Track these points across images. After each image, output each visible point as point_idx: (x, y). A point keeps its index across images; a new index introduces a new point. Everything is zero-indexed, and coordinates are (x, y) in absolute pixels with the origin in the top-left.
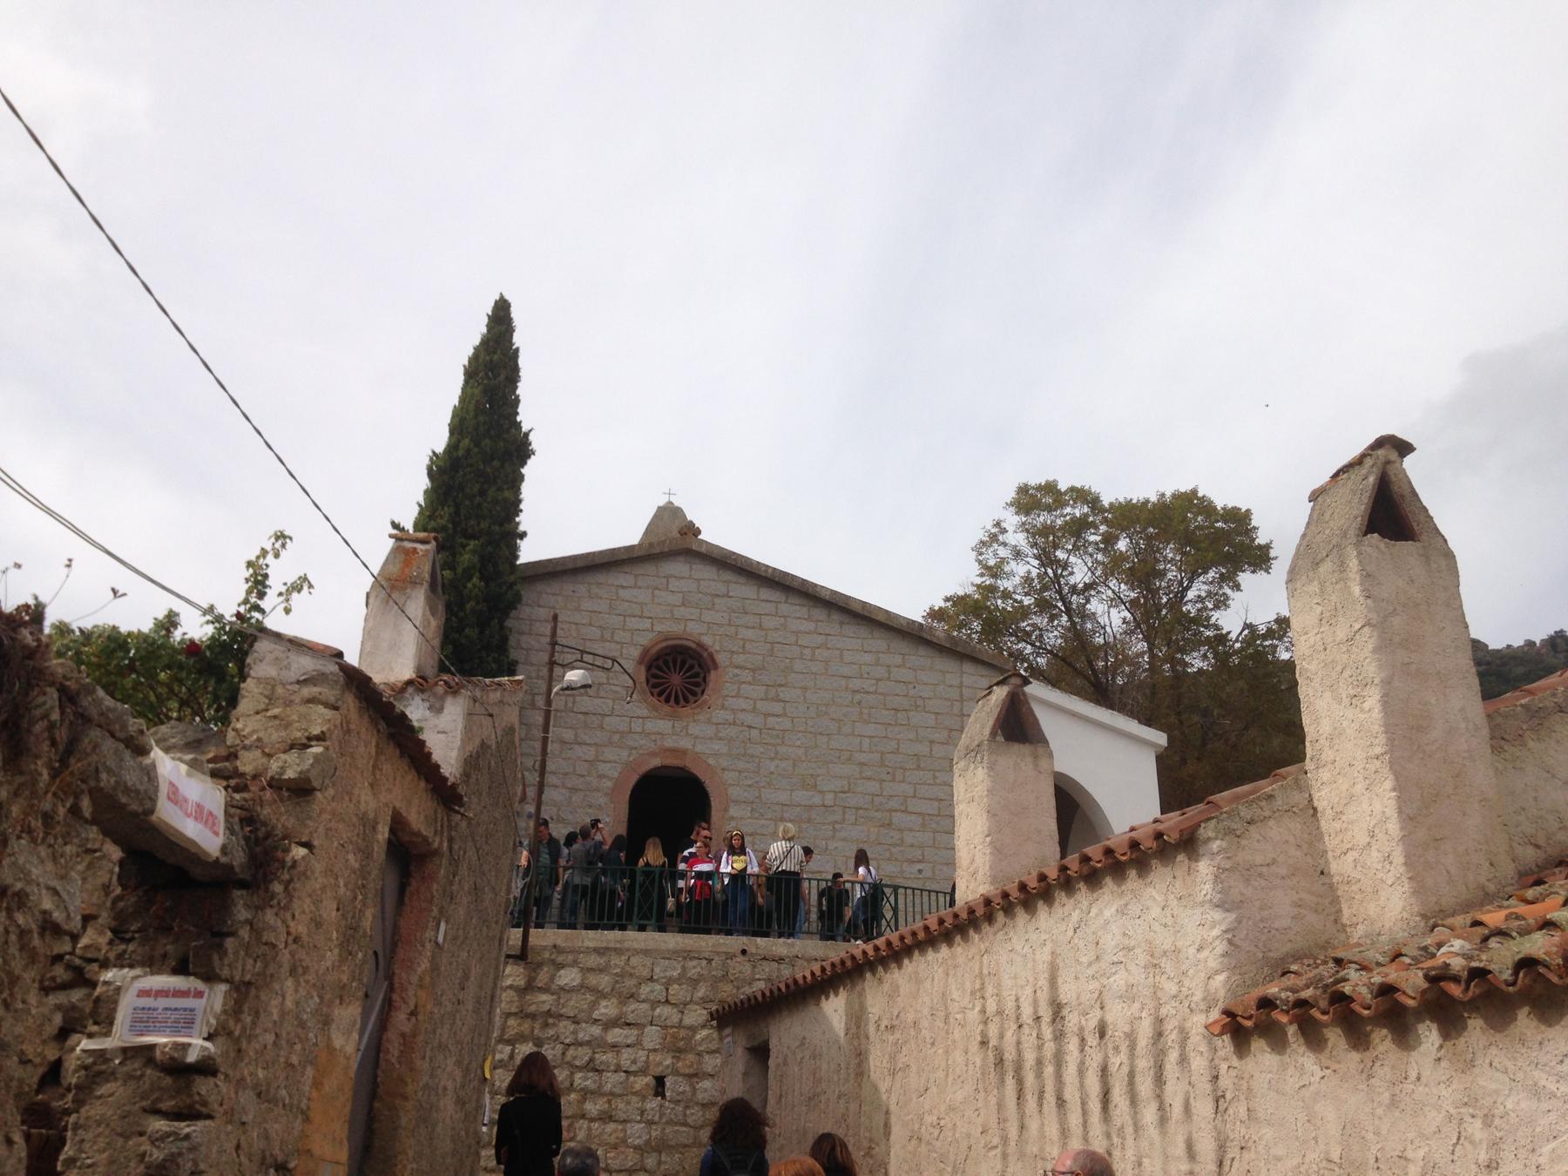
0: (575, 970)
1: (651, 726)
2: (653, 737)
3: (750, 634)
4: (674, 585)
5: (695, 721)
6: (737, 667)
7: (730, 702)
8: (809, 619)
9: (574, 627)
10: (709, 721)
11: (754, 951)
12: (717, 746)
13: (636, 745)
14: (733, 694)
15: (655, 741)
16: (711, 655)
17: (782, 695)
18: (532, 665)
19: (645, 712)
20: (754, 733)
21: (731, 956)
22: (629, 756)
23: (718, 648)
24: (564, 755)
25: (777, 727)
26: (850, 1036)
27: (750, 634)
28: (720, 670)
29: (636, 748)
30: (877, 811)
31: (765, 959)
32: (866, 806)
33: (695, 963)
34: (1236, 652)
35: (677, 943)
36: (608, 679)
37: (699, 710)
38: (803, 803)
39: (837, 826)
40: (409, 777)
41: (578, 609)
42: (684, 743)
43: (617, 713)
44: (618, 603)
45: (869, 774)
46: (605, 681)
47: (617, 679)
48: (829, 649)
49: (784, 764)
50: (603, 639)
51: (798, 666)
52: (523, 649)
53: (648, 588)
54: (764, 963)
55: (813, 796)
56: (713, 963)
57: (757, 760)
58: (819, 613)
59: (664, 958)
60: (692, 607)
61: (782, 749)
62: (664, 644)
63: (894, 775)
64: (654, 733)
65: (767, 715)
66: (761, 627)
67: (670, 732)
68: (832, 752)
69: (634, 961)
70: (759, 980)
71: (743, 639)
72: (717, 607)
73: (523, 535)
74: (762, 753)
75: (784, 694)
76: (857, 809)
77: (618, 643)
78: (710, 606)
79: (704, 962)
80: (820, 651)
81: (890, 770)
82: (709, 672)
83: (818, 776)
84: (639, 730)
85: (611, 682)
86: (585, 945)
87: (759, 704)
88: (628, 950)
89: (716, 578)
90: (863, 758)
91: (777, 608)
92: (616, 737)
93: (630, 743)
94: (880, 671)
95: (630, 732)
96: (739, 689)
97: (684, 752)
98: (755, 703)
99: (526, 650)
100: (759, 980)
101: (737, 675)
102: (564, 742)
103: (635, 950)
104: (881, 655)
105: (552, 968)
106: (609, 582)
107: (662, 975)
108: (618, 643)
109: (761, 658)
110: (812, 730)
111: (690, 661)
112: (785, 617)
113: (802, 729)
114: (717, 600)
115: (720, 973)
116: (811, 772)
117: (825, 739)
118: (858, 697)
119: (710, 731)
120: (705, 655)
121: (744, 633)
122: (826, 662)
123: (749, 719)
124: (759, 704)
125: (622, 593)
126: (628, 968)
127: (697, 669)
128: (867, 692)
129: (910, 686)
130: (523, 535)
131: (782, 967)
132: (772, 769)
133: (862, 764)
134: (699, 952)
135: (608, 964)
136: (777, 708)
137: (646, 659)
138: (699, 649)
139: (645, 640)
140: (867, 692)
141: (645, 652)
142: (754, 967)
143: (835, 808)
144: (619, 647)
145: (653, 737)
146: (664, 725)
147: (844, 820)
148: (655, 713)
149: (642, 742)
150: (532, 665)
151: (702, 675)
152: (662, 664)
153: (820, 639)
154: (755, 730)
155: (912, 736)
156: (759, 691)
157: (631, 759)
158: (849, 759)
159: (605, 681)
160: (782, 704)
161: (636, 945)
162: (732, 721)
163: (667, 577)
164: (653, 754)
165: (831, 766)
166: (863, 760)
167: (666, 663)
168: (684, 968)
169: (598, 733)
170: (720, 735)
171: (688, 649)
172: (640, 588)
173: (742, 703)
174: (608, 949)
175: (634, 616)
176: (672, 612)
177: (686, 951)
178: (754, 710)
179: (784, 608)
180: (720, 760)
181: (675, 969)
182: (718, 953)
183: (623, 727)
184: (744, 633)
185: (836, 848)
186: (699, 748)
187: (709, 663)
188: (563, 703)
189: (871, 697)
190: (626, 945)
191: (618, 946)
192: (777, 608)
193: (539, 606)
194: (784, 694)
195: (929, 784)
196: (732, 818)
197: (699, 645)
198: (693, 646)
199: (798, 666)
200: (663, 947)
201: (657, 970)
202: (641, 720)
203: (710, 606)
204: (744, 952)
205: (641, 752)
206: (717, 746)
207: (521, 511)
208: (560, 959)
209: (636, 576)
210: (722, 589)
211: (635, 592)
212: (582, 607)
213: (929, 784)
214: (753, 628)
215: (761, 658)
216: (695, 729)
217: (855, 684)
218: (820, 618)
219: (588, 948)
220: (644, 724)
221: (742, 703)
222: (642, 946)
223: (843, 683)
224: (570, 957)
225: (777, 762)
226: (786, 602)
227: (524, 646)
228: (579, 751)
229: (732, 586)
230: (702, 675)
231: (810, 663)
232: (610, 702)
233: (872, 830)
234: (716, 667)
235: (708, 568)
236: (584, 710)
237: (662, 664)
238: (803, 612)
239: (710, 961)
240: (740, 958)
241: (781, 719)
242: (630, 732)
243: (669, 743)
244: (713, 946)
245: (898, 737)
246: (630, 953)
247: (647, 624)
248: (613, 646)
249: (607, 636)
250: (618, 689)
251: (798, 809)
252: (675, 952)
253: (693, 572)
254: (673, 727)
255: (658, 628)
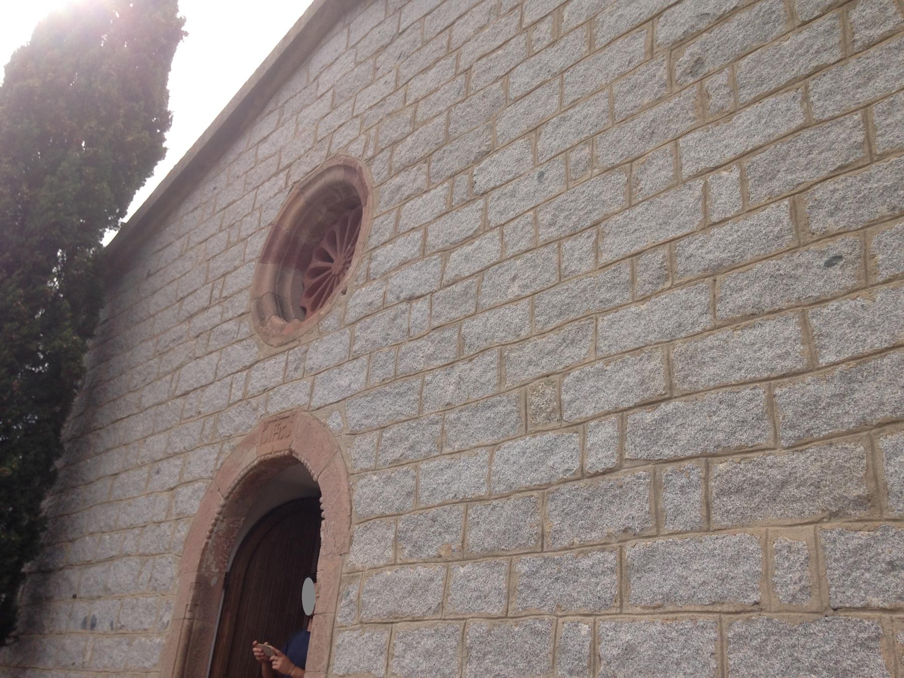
26: (473, 241)
30: (798, 446)
32: (744, 437)
34: (59, 291)
38: (523, 483)
39: (633, 550)
40: (139, 426)
45: (746, 297)
55: (550, 451)
62: (301, 202)
63: (866, 257)
74: (430, 357)
76: (708, 457)
81: (838, 246)
117: (584, 243)
118: (686, 56)
133: (714, 272)
143: (625, 477)
147: (657, 515)
185: (629, 650)
196: (354, 574)
207: (165, 149)
233: (784, 539)
251: (508, 508)
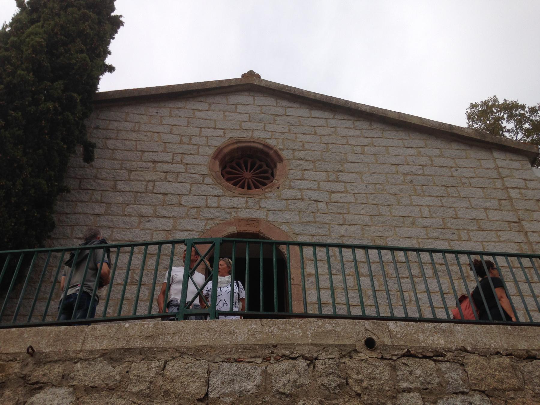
0: (63, 391)
1: (226, 202)
2: (228, 210)
3: (308, 138)
4: (240, 109)
5: (266, 197)
6: (299, 160)
7: (297, 183)
8: (355, 128)
9: (156, 135)
10: (279, 198)
11: (387, 341)
12: (288, 216)
13: (212, 217)
14: (299, 178)
15: (230, 213)
16: (276, 152)
17: (341, 178)
18: (116, 160)
19: (220, 192)
20: (321, 206)
21: (351, 352)
22: (205, 225)
23: (281, 147)
24: (141, 227)
25: (341, 200)
27: (308, 138)
28: (284, 161)
29: (212, 219)
31: (409, 355)
33: (286, 365)
35: (251, 333)
36: (186, 169)
37: (269, 189)
41: (160, 123)
42: (256, 214)
43: (194, 193)
44: (194, 120)
46: (183, 170)
47: (194, 169)
48: (375, 146)
49: (353, 229)
50: (181, 142)
51: (351, 157)
52: (108, 149)
53: (220, 111)
54: (410, 361)
56: (319, 365)
57: (327, 226)
58: (363, 124)
59: (228, 360)
60: (257, 122)
61: (350, 217)
62: (236, 146)
64: (229, 208)
65: (331, 192)
66: (315, 134)
67: (244, 206)
68: (394, 218)
69: (172, 369)
70: (408, 390)
71: (302, 141)
72: (277, 122)
73: (110, 53)
74: (331, 220)
75: (343, 177)
77: (196, 145)
78: (272, 122)
79: (302, 364)
80: (369, 147)
81: (454, 231)
82: (275, 166)
83: (387, 237)
84: (216, 205)
85: (189, 171)
86: (88, 347)
87: (322, 185)
88: (164, 350)
89: (275, 105)
90: (425, 222)
91: (327, 122)
92: (193, 211)
93: (208, 215)
94: (424, 160)
95: (207, 206)
96: (303, 174)
97: (257, 221)
98: (319, 184)
99: (113, 150)
100: (408, 390)
101: (301, 165)
102: (143, 216)
103: (177, 350)
104: (421, 149)
105: (21, 391)
106: (188, 107)
107: (227, 390)
108: (196, 145)
109: (319, 153)
110: (374, 202)
111: (258, 163)
112: (335, 127)
113: (364, 201)
114: (277, 118)
115: (334, 381)
116: (379, 234)
118: (408, 178)
119: (281, 205)
120: (271, 152)
121: (301, 137)
122: (375, 155)
123: (315, 195)
124: (322, 185)
125: (198, 114)
126: (160, 381)
127: (265, 167)
128: (416, 175)
129: (454, 169)
130: (110, 53)
131: (444, 367)
132: (343, 232)
134: (291, 346)
135: (125, 376)
136: (339, 187)
137: (220, 156)
138: (266, 149)
139: (219, 142)
140: (416, 175)
141: (220, 150)
142: (394, 368)
144: (195, 147)
145: (228, 210)
146: (239, 201)
148: (230, 193)
149: (217, 214)
150: (116, 160)
151: (270, 172)
152: (235, 165)
153: (367, 141)
154: (321, 203)
155: (464, 204)
156: (322, 176)
157: (208, 227)
158: (413, 223)
159: (183, 170)
160: (343, 184)
161: (177, 342)
162: (300, 197)
163: (236, 105)
164: (230, 224)
165: (397, 229)
166: (427, 224)
167: (239, 165)
168: (265, 373)
169: (177, 209)
170: (290, 207)
171: (256, 150)
172: (213, 111)
173: (306, 184)
174: (127, 351)
175: (209, 128)
176: (240, 125)
177: (267, 346)
178: (319, 189)
179: (333, 122)
180: (292, 227)
181: (249, 377)
182: (325, 348)
183: (201, 203)
184: (301, 137)
186: (271, 218)
187: (276, 158)
188: (144, 187)
189: (420, 178)
190: (161, 343)
191: (147, 344)
192: (327, 122)
193: (126, 121)
194: (343, 177)
195: (495, 242)
197: (265, 145)
198: (260, 147)
199: (351, 157)
200: (226, 340)
201: (216, 381)
202: (216, 198)
203: (272, 122)
204: (370, 344)
205: (217, 222)
206: (288, 216)
208: (38, 374)
209: (210, 104)
210: (281, 111)
211: (209, 113)
212: (164, 122)
213: (495, 242)
214: (310, 134)
215: (319, 153)
216: (266, 204)
217: (406, 169)
218: (364, 127)
219: (91, 352)
220: (219, 201)
221: (306, 184)
222: (190, 341)
223: (393, 168)
224: (58, 369)
225: (345, 227)
226: (334, 118)
227: (110, 147)
228: (157, 223)
229: (288, 110)
230: (270, 172)
231: (361, 156)
232: (188, 186)
234: (281, 159)
235: (268, 99)
236: (162, 191)
237: (235, 165)
238: (349, 124)
239: (312, 361)
240: (365, 354)
241: (344, 195)
242: (207, 206)
243: (243, 214)
244: (315, 336)
245: (454, 205)
246: (166, 356)
247: (220, 132)
248: (191, 147)
249: (185, 140)
250: (197, 176)
252: (248, 348)
253: (256, 101)
254: (247, 201)
255: (229, 135)
